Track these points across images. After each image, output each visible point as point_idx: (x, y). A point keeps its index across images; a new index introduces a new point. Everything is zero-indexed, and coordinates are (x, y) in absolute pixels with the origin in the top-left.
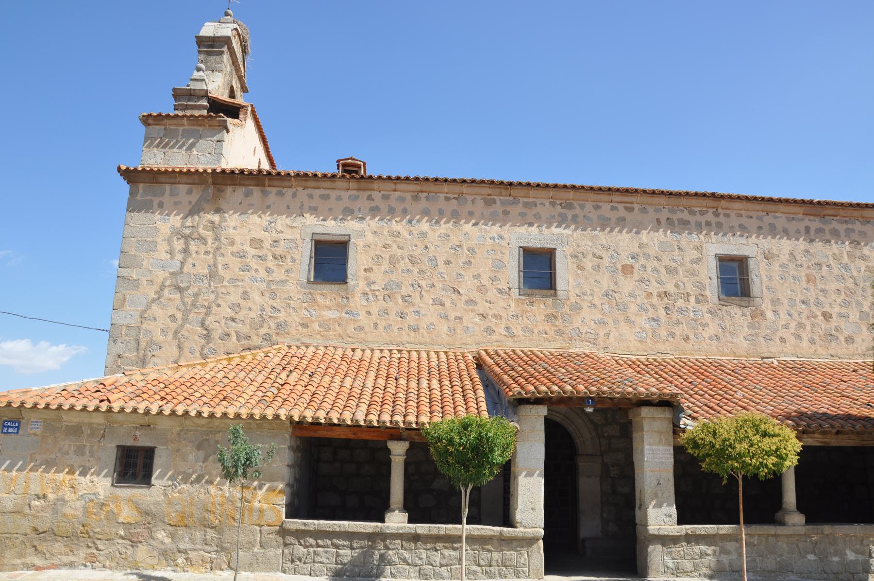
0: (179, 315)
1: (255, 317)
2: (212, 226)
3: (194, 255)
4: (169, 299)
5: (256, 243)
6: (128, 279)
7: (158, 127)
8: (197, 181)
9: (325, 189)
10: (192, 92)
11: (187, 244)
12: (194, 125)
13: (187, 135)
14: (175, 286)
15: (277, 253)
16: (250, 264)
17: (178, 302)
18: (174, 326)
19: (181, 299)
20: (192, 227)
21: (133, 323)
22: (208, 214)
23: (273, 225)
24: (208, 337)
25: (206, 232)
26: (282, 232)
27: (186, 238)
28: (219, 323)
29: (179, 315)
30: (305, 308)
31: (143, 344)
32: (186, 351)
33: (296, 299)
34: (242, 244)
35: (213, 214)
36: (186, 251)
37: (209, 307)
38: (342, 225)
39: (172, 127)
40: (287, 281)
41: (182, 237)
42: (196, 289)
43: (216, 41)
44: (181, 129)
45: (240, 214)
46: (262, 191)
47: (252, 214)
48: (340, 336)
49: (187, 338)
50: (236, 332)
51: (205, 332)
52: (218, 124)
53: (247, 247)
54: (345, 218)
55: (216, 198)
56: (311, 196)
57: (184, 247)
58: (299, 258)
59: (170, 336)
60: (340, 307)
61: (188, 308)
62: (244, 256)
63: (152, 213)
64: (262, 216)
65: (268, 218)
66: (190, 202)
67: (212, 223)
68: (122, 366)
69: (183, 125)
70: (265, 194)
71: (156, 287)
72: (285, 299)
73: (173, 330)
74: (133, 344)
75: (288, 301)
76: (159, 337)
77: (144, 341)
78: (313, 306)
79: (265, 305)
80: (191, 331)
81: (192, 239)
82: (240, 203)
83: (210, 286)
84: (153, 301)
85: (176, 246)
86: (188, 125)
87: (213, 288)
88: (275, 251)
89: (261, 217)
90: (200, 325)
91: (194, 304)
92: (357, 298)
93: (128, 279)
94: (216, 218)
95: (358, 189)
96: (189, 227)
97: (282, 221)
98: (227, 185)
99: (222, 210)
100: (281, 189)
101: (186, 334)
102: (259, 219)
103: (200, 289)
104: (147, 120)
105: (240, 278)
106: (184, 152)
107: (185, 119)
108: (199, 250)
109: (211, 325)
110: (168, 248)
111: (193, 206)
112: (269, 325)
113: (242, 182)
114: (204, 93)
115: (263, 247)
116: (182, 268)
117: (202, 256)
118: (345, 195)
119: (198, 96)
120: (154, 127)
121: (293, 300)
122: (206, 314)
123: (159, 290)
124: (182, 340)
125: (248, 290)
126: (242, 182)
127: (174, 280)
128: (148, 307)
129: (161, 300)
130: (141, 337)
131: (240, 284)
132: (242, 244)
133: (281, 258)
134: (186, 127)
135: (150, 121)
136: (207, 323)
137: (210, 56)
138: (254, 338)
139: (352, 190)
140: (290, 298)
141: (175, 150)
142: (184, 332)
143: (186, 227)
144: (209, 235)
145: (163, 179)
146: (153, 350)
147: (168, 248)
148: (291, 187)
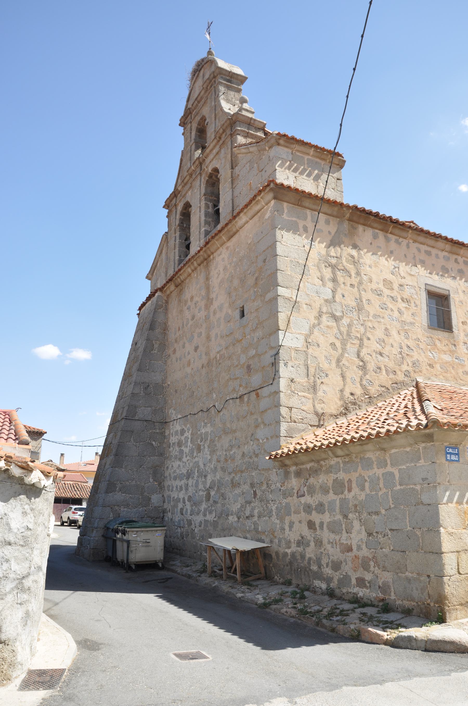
0: (338, 344)
1: (397, 354)
2: (354, 262)
3: (342, 286)
4: (328, 327)
5: (388, 283)
6: (289, 299)
7: (286, 149)
8: (335, 213)
9: (427, 245)
10: (252, 122)
11: (334, 273)
12: (317, 157)
13: (314, 166)
14: (331, 315)
15: (404, 297)
16: (387, 303)
17: (335, 330)
18: (336, 354)
19: (338, 328)
20: (336, 257)
21: (300, 347)
22: (348, 247)
23: (397, 269)
24: (363, 368)
25: (348, 265)
26: (404, 278)
27: (333, 267)
28: (371, 355)
29: (338, 344)
30: (430, 350)
31: (312, 370)
32: (348, 380)
33: (422, 341)
34: (378, 283)
35: (352, 249)
36: (334, 280)
37: (361, 340)
38: (443, 281)
39: (298, 154)
40: (414, 323)
41: (329, 266)
42: (348, 320)
43: (233, 78)
44: (306, 157)
45: (373, 254)
46: (385, 236)
47: (381, 256)
48: (455, 378)
49: (348, 368)
50: (385, 366)
51: (361, 364)
52: (337, 163)
53: (381, 286)
54: (444, 275)
55: (352, 233)
56: (419, 250)
57: (332, 276)
58: (419, 304)
59: (334, 364)
60: (452, 353)
61: (345, 337)
62: (381, 295)
63: (299, 235)
64: (389, 259)
65: (393, 263)
66: (329, 232)
67: (353, 257)
68: (296, 392)
69: (308, 154)
70: (387, 240)
71: (315, 313)
72: (415, 339)
73: (336, 359)
74: (302, 370)
75: (417, 342)
76: (325, 365)
77: (313, 367)
78: (434, 349)
79: (402, 343)
80: (350, 361)
81: (338, 269)
82: (371, 244)
83: (359, 319)
84: (314, 326)
85: (325, 274)
86: (312, 156)
87: (362, 322)
88: (403, 294)
89: (388, 261)
90: (356, 356)
91: (349, 335)
92: (460, 346)
93: (289, 299)
94: (354, 252)
95: (451, 252)
96: (334, 257)
97: (404, 268)
98: (358, 223)
99: (358, 246)
100: (398, 238)
101: (346, 363)
102: (386, 262)
103: (351, 321)
104: (279, 139)
105: (381, 315)
106: (312, 181)
107: (313, 149)
108: (346, 282)
109: (365, 357)
110: (319, 274)
111: (333, 237)
112: (408, 363)
113: (372, 224)
114: (262, 126)
115: (393, 289)
116: (334, 297)
117: (348, 287)
118: (442, 254)
119: (255, 128)
120: (282, 148)
121: (421, 342)
122: (360, 346)
123: (317, 315)
124: (345, 369)
125: (389, 327)
126: (372, 224)
127: (329, 307)
128: (311, 332)
129: (321, 326)
130: (309, 362)
131: (382, 320)
132: (378, 283)
133: (407, 302)
134: (310, 157)
135: (281, 142)
136: (362, 354)
137: (230, 90)
138: (399, 373)
139: (445, 251)
140: (418, 340)
141: (304, 177)
142: (344, 361)
143: (331, 257)
144: (350, 267)
145: (307, 203)
146: (321, 377)
147: (319, 274)
148: (405, 238)
